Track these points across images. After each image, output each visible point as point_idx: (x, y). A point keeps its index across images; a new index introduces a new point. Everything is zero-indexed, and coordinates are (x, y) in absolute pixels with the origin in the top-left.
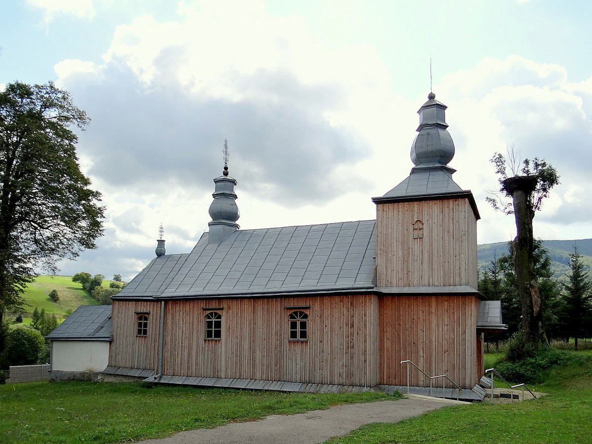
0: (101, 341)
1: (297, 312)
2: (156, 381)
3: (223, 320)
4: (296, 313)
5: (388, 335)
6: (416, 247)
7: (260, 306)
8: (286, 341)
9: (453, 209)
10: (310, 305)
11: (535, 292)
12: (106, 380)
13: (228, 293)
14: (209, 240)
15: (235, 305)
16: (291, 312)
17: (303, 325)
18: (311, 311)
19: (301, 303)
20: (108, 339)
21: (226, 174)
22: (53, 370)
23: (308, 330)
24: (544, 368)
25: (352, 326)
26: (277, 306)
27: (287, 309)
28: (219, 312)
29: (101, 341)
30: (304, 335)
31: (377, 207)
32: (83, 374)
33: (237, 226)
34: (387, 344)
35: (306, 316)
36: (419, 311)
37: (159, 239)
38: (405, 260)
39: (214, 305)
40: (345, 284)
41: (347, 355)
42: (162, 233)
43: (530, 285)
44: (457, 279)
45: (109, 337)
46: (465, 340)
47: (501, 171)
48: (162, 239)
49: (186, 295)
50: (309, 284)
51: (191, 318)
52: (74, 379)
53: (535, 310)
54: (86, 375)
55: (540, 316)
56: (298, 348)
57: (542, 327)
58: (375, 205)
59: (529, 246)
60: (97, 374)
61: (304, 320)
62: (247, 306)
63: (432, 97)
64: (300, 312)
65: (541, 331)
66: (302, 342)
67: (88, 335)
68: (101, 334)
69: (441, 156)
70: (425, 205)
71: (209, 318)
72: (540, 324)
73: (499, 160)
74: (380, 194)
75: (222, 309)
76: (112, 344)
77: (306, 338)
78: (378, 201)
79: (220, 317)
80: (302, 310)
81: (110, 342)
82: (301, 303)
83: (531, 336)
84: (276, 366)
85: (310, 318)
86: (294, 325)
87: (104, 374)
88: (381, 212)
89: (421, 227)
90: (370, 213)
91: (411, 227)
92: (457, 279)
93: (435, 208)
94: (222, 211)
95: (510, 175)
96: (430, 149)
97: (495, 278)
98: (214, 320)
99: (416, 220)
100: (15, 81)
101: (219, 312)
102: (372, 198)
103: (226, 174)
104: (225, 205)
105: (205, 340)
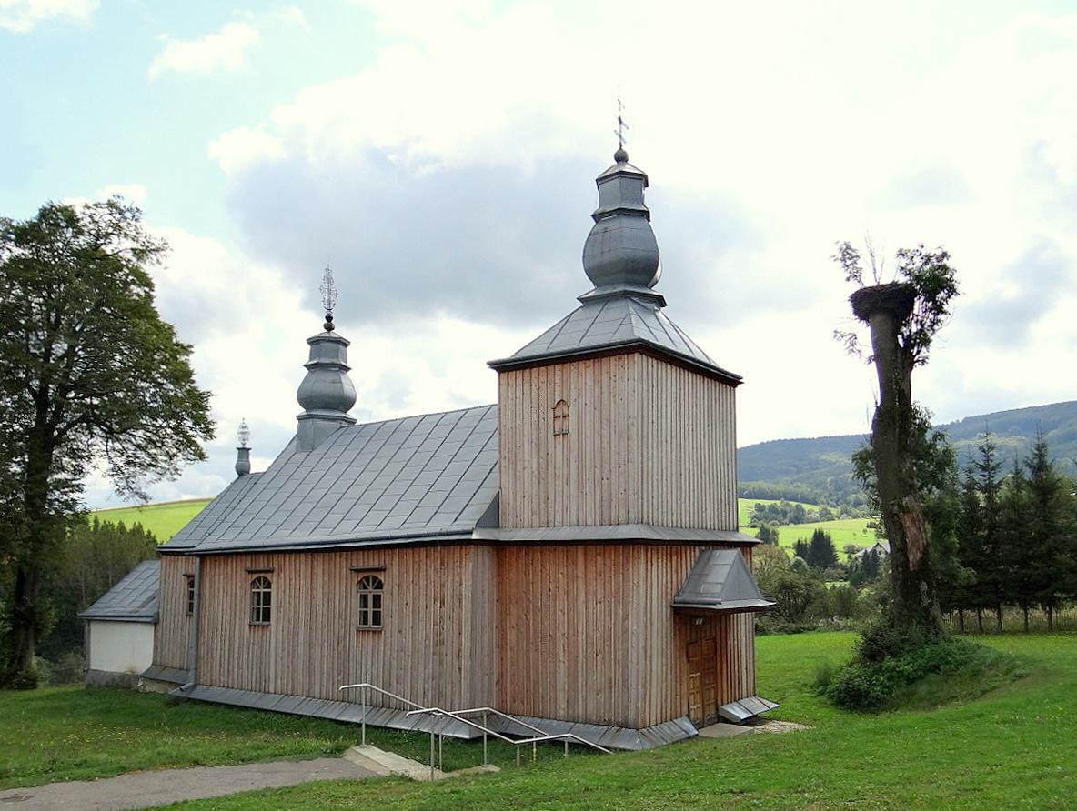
0: (145, 622)
1: (368, 576)
2: (184, 695)
3: (273, 590)
4: (367, 578)
5: (511, 621)
6: (557, 449)
7: (321, 564)
8: (353, 630)
9: (615, 376)
10: (385, 565)
11: (913, 520)
12: (148, 689)
13: (262, 544)
14: (305, 441)
15: (288, 563)
16: (362, 575)
17: (377, 599)
18: (387, 575)
19: (373, 561)
20: (149, 620)
21: (329, 328)
22: (92, 668)
23: (385, 609)
24: (911, 681)
25: (442, 603)
26: (342, 565)
27: (356, 571)
28: (268, 576)
29: (145, 622)
30: (377, 620)
31: (499, 377)
32: (123, 676)
33: (352, 422)
34: (511, 636)
35: (380, 586)
36: (556, 573)
37: (241, 446)
38: (541, 477)
39: (262, 564)
40: (442, 524)
41: (591, 641)
42: (246, 436)
43: (900, 506)
44: (622, 512)
45: (151, 616)
46: (626, 631)
47: (856, 276)
48: (247, 446)
49: (224, 547)
50: (393, 527)
51: (234, 587)
52: (106, 686)
53: (911, 559)
54: (126, 679)
55: (924, 569)
56: (369, 641)
57: (929, 593)
58: (494, 373)
59: (900, 427)
60: (138, 677)
61: (378, 592)
62: (303, 564)
63: (621, 158)
64: (373, 577)
65: (926, 601)
66: (374, 632)
67: (131, 612)
68: (144, 611)
69: (628, 271)
70: (572, 370)
71: (365, 588)
72: (924, 586)
73: (848, 255)
74: (506, 353)
75: (272, 571)
76: (158, 628)
77: (380, 624)
78: (502, 367)
79: (269, 586)
80: (375, 574)
81: (156, 624)
82: (373, 561)
83: (905, 612)
84: (339, 674)
85: (386, 587)
86: (364, 598)
87: (147, 677)
88: (504, 388)
89: (566, 413)
90: (487, 389)
91: (551, 414)
92: (622, 512)
93: (582, 379)
94: (313, 395)
95: (869, 282)
96: (607, 258)
97: (989, 479)
98: (262, 590)
99: (557, 400)
100: (48, 201)
101: (268, 576)
102: (488, 364)
103: (329, 328)
104: (324, 383)
105: (250, 626)
